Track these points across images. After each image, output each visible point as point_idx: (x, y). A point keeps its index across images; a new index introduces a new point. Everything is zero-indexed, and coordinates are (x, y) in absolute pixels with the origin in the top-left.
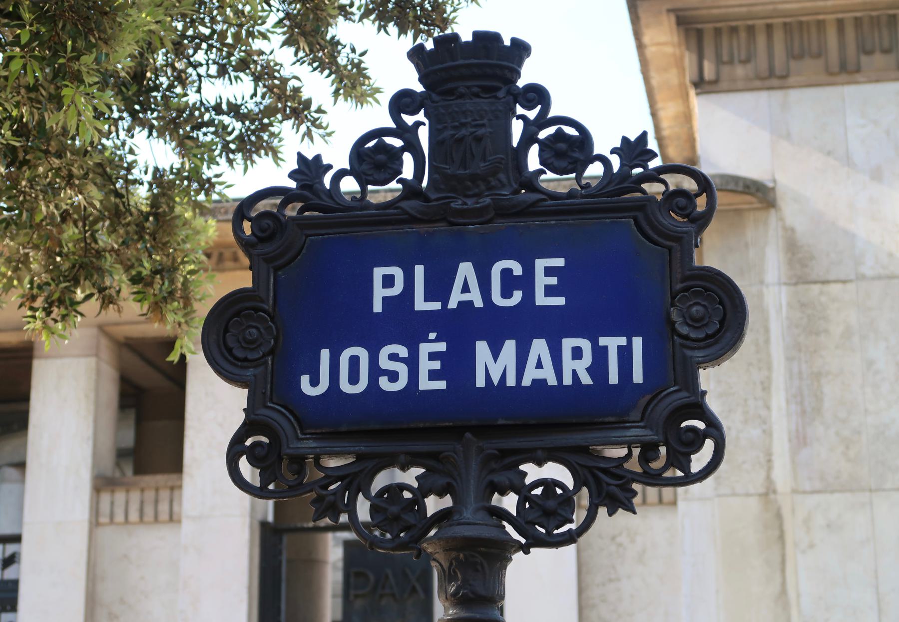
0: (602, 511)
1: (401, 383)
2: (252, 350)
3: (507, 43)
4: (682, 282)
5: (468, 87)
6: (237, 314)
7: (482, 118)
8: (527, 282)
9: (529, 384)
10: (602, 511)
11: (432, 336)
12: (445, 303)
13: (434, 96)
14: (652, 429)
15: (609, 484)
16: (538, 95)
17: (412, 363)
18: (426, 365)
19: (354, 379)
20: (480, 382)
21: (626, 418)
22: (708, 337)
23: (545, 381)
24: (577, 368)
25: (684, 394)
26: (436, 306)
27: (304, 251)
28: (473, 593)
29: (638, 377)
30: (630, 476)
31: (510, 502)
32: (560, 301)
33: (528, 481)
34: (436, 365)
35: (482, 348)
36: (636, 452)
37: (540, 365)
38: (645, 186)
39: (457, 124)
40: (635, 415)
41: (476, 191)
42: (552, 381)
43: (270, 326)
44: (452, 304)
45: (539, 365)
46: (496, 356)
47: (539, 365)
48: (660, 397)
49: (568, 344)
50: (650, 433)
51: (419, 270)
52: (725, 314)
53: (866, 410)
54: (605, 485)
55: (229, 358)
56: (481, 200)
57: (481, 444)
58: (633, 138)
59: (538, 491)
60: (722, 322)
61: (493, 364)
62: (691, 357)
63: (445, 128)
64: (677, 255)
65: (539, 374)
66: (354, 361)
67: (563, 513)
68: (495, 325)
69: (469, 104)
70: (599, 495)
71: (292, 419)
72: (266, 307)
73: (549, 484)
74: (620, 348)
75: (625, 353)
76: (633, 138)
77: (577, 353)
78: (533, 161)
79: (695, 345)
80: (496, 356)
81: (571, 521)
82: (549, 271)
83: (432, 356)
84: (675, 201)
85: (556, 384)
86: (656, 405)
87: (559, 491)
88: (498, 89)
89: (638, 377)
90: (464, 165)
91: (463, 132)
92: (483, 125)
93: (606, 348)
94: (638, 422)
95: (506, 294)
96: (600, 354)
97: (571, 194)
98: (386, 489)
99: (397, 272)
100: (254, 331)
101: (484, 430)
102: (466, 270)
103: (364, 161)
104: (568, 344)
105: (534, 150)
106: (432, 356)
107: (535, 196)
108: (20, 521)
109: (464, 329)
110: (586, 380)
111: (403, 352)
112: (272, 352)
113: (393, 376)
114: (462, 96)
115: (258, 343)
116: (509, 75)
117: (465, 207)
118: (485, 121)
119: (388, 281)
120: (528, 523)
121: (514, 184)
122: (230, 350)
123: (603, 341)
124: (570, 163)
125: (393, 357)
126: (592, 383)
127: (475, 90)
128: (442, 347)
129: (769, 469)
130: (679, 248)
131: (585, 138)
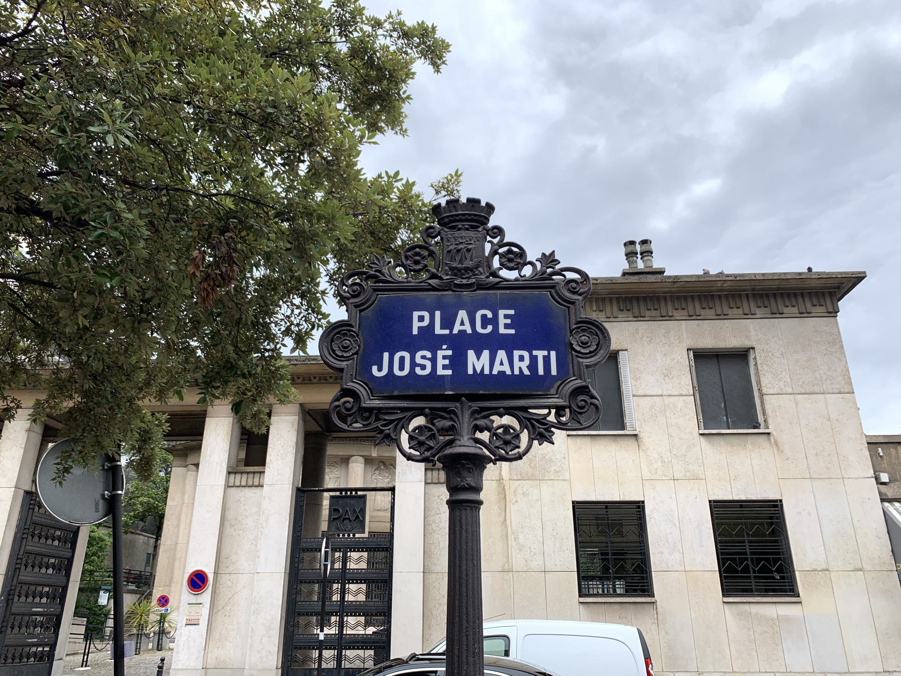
0: (536, 442)
3: (483, 204)
6: (339, 333)
8: (494, 321)
10: (536, 442)
11: (444, 347)
12: (451, 330)
16: (498, 231)
17: (434, 360)
18: (441, 362)
19: (402, 368)
20: (470, 371)
22: (591, 352)
24: (522, 366)
25: (579, 381)
26: (447, 332)
29: (554, 372)
31: (485, 436)
32: (512, 331)
33: (495, 425)
35: (471, 354)
36: (553, 411)
40: (553, 391)
42: (509, 372)
44: (455, 331)
45: (502, 364)
47: (502, 364)
49: (517, 353)
51: (438, 314)
59: (500, 431)
60: (597, 345)
61: (477, 362)
64: (572, 311)
65: (502, 368)
66: (402, 359)
68: (479, 343)
69: (463, 233)
70: (534, 433)
73: (506, 428)
74: (544, 356)
75: (547, 359)
77: (521, 358)
78: (496, 262)
81: (519, 447)
82: (506, 316)
83: (444, 357)
89: (554, 372)
90: (461, 262)
91: (461, 246)
95: (484, 326)
96: (534, 359)
97: (516, 280)
99: (426, 315)
101: (472, 398)
102: (462, 314)
105: (497, 257)
106: (444, 357)
109: (461, 345)
110: (526, 372)
111: (429, 355)
112: (356, 353)
113: (423, 367)
114: (460, 229)
119: (421, 319)
122: (334, 351)
123: (535, 353)
125: (423, 357)
128: (449, 353)
131: (522, 253)
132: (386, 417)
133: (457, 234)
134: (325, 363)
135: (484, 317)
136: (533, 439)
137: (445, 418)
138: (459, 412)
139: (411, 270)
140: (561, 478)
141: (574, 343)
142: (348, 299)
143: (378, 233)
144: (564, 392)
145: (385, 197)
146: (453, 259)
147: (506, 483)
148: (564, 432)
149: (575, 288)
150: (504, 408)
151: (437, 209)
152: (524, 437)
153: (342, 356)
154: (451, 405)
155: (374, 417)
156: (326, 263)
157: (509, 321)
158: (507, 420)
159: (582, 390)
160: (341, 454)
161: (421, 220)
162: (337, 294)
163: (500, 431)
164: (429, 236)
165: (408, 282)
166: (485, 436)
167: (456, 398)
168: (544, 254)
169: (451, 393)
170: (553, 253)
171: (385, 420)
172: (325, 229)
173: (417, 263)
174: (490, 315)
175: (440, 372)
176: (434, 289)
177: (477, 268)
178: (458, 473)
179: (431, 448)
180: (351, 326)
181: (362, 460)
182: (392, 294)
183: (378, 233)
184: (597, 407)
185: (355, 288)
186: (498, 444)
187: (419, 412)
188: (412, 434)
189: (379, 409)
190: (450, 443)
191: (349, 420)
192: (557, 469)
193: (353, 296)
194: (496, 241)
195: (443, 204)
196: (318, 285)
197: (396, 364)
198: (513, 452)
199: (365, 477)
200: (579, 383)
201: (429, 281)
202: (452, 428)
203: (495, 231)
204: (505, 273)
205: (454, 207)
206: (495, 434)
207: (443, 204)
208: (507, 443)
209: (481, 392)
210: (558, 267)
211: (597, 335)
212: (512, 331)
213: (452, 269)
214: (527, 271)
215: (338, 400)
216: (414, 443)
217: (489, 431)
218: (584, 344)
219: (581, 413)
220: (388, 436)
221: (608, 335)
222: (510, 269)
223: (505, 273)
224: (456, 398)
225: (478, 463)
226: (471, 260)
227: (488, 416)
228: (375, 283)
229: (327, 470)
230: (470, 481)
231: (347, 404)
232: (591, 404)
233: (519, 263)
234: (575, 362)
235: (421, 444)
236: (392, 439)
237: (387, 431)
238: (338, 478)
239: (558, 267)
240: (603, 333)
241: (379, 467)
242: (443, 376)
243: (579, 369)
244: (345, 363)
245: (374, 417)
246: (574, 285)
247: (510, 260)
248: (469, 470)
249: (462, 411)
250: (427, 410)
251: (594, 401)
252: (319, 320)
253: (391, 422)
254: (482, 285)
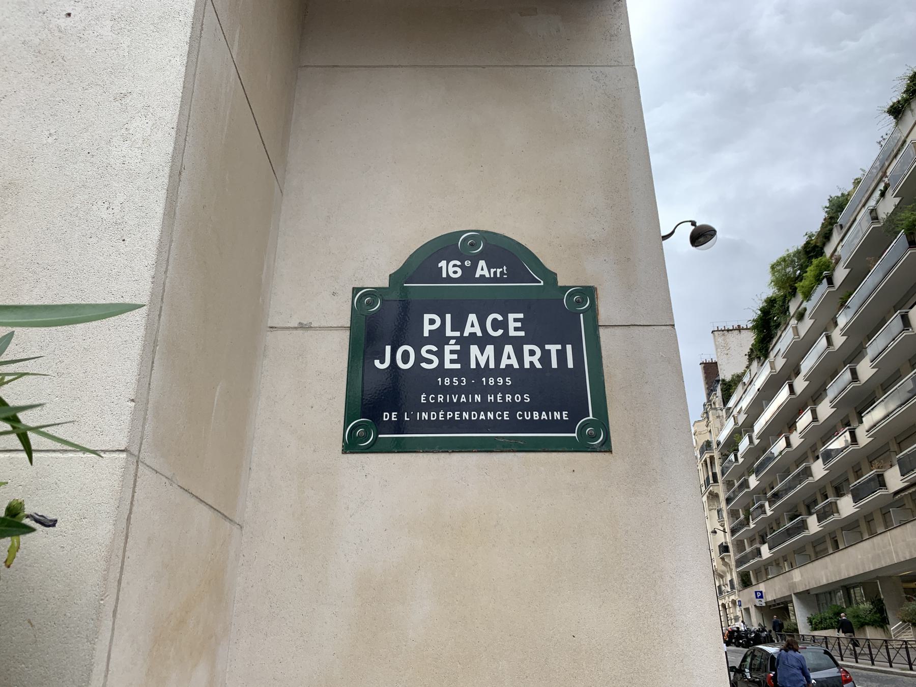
12: (462, 333)
18: (448, 357)
26: (458, 334)
44: (466, 334)
47: (509, 357)
49: (527, 348)
51: (448, 317)
75: (562, 355)
82: (516, 320)
83: (452, 352)
96: (546, 355)
102: (472, 317)
104: (527, 348)
106: (452, 352)
108: (672, 319)
119: (432, 322)
123: (547, 347)
174: (500, 318)
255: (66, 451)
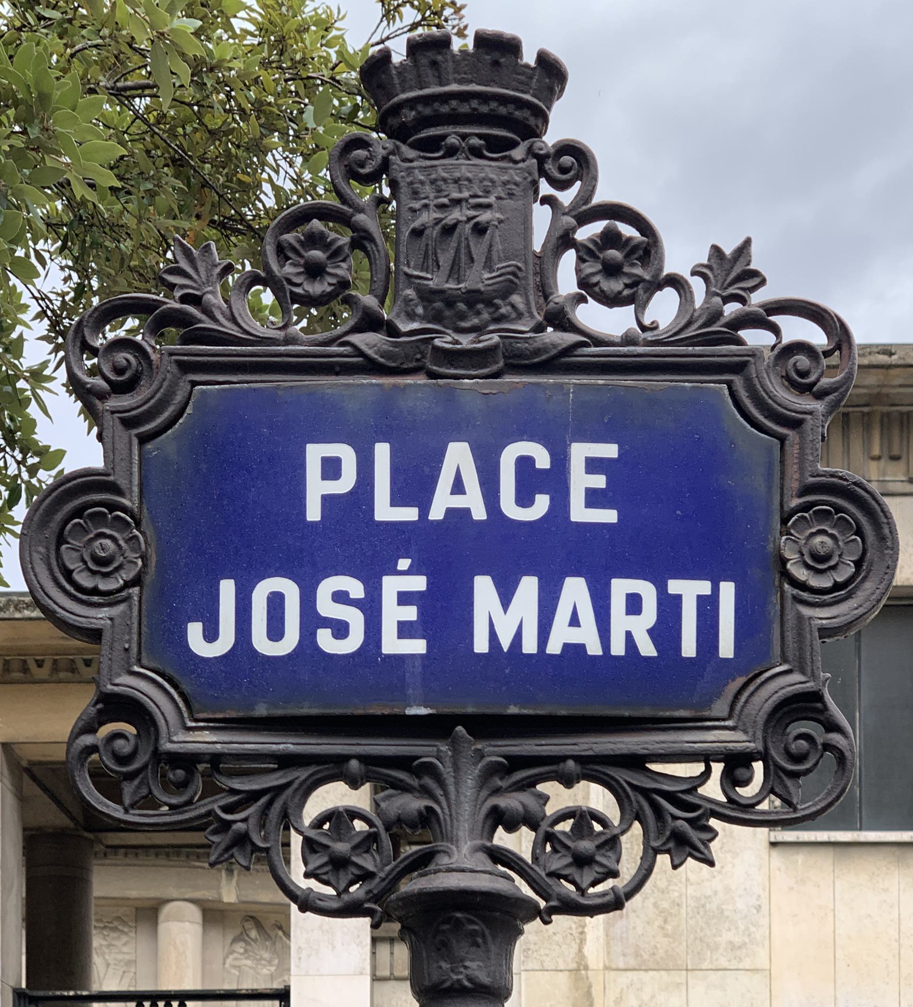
0: (663, 860)
1: (353, 643)
2: (106, 575)
3: (529, 58)
4: (800, 495)
5: (464, 137)
6: (78, 512)
7: (487, 193)
8: (555, 481)
9: (558, 651)
10: (663, 860)
11: (404, 564)
12: (424, 510)
13: (404, 148)
14: (745, 732)
15: (675, 818)
16: (576, 161)
17: (371, 608)
18: (394, 614)
19: (276, 631)
20: (481, 645)
21: (706, 714)
22: (837, 587)
23: (581, 648)
24: (634, 630)
25: (796, 677)
26: (410, 514)
27: (189, 410)
28: (470, 980)
29: (726, 648)
30: (709, 806)
31: (520, 842)
32: (609, 516)
33: (550, 810)
34: (410, 613)
35: (484, 588)
36: (717, 768)
37: (575, 622)
38: (743, 334)
39: (445, 201)
40: (720, 708)
41: (476, 321)
42: (594, 648)
43: (136, 537)
44: (437, 513)
45: (574, 621)
46: (506, 601)
47: (574, 621)
48: (759, 681)
49: (620, 588)
50: (744, 737)
51: (382, 452)
52: (865, 552)
53: (687, 880)
54: (670, 819)
55: (68, 587)
56: (482, 338)
57: (479, 746)
58: (728, 250)
59: (566, 826)
60: (858, 564)
61: (501, 616)
62: (810, 618)
63: (426, 206)
64: (793, 450)
65: (574, 636)
66: (276, 602)
67: (604, 861)
68: (511, 552)
69: (463, 166)
70: (660, 833)
71: (176, 696)
72: (126, 502)
73: (583, 818)
74: (700, 599)
75: (708, 608)
76: (728, 250)
77: (634, 604)
78: (566, 276)
79: (817, 598)
80: (506, 601)
81: (615, 874)
82: (593, 466)
83: (404, 598)
84: (792, 361)
85: (600, 653)
86: (752, 694)
87: (597, 827)
88: (514, 145)
89: (726, 648)
90: (455, 271)
91: (456, 215)
92: (489, 206)
93: (679, 598)
94: (724, 720)
95: (524, 499)
96: (670, 607)
97: (628, 340)
98: (331, 816)
99: (346, 454)
100: (108, 542)
101: (486, 726)
102: (458, 456)
103: (288, 258)
104: (620, 588)
105: (570, 257)
106: (404, 598)
107: (572, 338)
109: (454, 555)
110: (647, 648)
111: (356, 588)
112: (136, 581)
113: (340, 630)
114: (452, 152)
115: (115, 565)
116: (532, 121)
117: (459, 347)
118: (492, 199)
119: (331, 468)
120: (551, 874)
121: (536, 314)
122: (68, 574)
123: (675, 586)
124: (627, 286)
125: (340, 597)
126: (655, 654)
127: (475, 141)
128: (419, 583)
129: (582, 942)
130: (797, 440)
131: (648, 248)
132: (236, 784)
133: (444, 167)
134: (50, 614)
135: (524, 464)
136: (657, 851)
137: (405, 788)
138: (446, 770)
139: (295, 298)
140: (746, 964)
141: (791, 554)
142: (102, 396)
143: (194, 161)
144: (752, 709)
145: (214, 26)
146: (429, 261)
147: (596, 980)
148: (763, 831)
149: (804, 374)
150: (578, 759)
151: (376, 68)
152: (633, 842)
153: (95, 591)
154: (424, 750)
155: (199, 782)
156: (28, 274)
157: (599, 481)
158: (596, 797)
159: (805, 705)
160: (134, 894)
161: (337, 117)
162: (75, 386)
163: (566, 826)
164: (352, 174)
165: (288, 341)
166: (520, 842)
167: (437, 727)
168: (716, 251)
169: (423, 711)
170: (745, 248)
171: (233, 792)
172: (19, 142)
173: (314, 271)
174: (543, 459)
175: (392, 644)
176: (371, 367)
177: (505, 294)
178: (443, 949)
179: (365, 876)
180: (115, 489)
181: (194, 912)
182: (240, 383)
183: (194, 161)
184: (842, 759)
185: (122, 357)
186: (558, 863)
187: (333, 769)
188: (312, 834)
189: (216, 759)
190: (422, 862)
191: (128, 789)
192: (737, 940)
193: (120, 389)
194: (567, 197)
195: (399, 53)
196: (15, 349)
197: (258, 618)
198: (600, 888)
199: (204, 962)
200: (795, 683)
201: (357, 339)
202: (427, 818)
203: (567, 160)
204: (595, 317)
205: (434, 64)
206: (549, 837)
207: (399, 53)
208: (582, 861)
209: (513, 710)
210: (758, 298)
211: (859, 532)
212: (609, 516)
213: (427, 296)
214: (664, 309)
215: (90, 728)
216: (318, 860)
217: (534, 827)
218: (819, 561)
219: (795, 775)
220: (242, 840)
221: (893, 531)
222: (611, 301)
223: (595, 317)
224: (437, 727)
225: (499, 918)
226: (488, 265)
227: (531, 783)
228: (185, 341)
229: (97, 941)
230: (477, 968)
231: (120, 743)
232: (827, 747)
233: (636, 282)
234: (790, 616)
235: (339, 863)
236: (256, 849)
237: (240, 826)
238: (129, 963)
239: (758, 298)
240: (877, 525)
241: (245, 931)
242: (400, 659)
243: (800, 635)
244: (104, 613)
245: (199, 782)
246: (803, 361)
247: (612, 270)
248: (474, 940)
249: (456, 768)
250: (354, 764)
251: (836, 738)
252: (33, 471)
253: (254, 796)
254: (520, 355)
255: (673, 742)
